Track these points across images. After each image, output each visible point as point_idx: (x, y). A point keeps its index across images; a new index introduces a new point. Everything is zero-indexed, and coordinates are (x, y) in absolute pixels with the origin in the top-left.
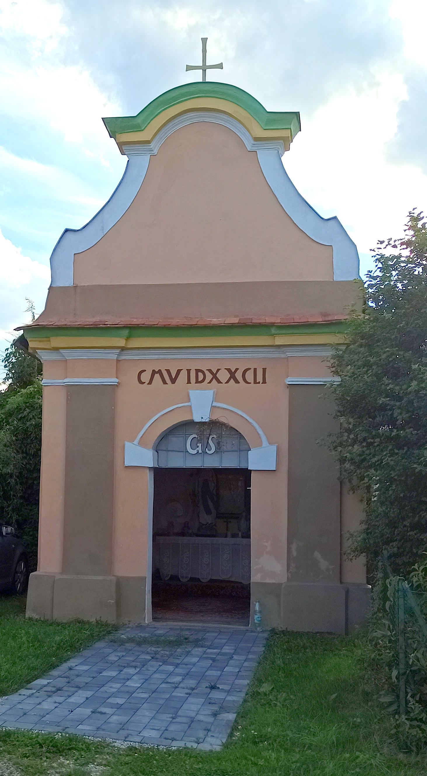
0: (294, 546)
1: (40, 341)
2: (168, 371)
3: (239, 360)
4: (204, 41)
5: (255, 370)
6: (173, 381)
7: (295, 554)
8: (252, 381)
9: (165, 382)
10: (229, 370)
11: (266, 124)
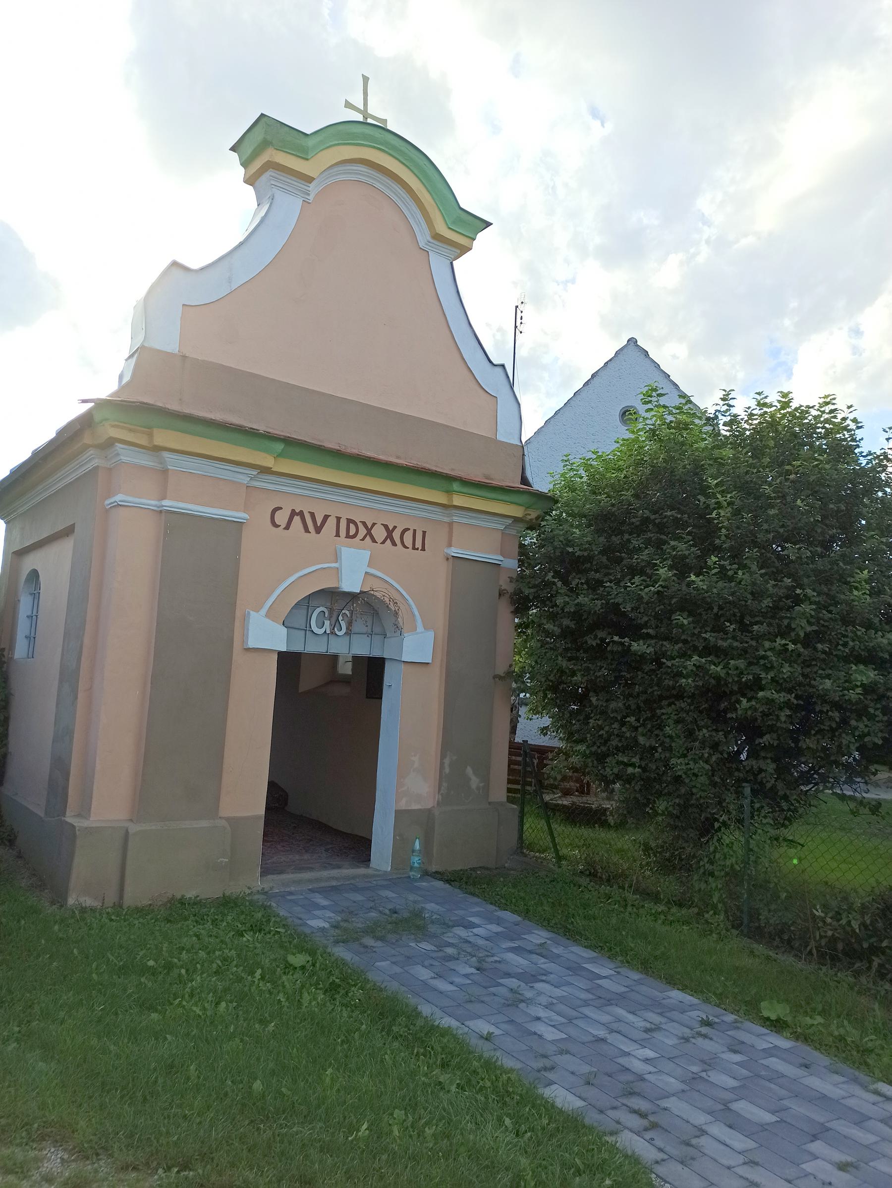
0: (447, 761)
1: (130, 430)
2: (312, 515)
3: (400, 516)
4: (366, 80)
5: (415, 531)
6: (318, 530)
7: (447, 770)
8: (410, 546)
9: (307, 530)
10: (386, 527)
11: (454, 223)
